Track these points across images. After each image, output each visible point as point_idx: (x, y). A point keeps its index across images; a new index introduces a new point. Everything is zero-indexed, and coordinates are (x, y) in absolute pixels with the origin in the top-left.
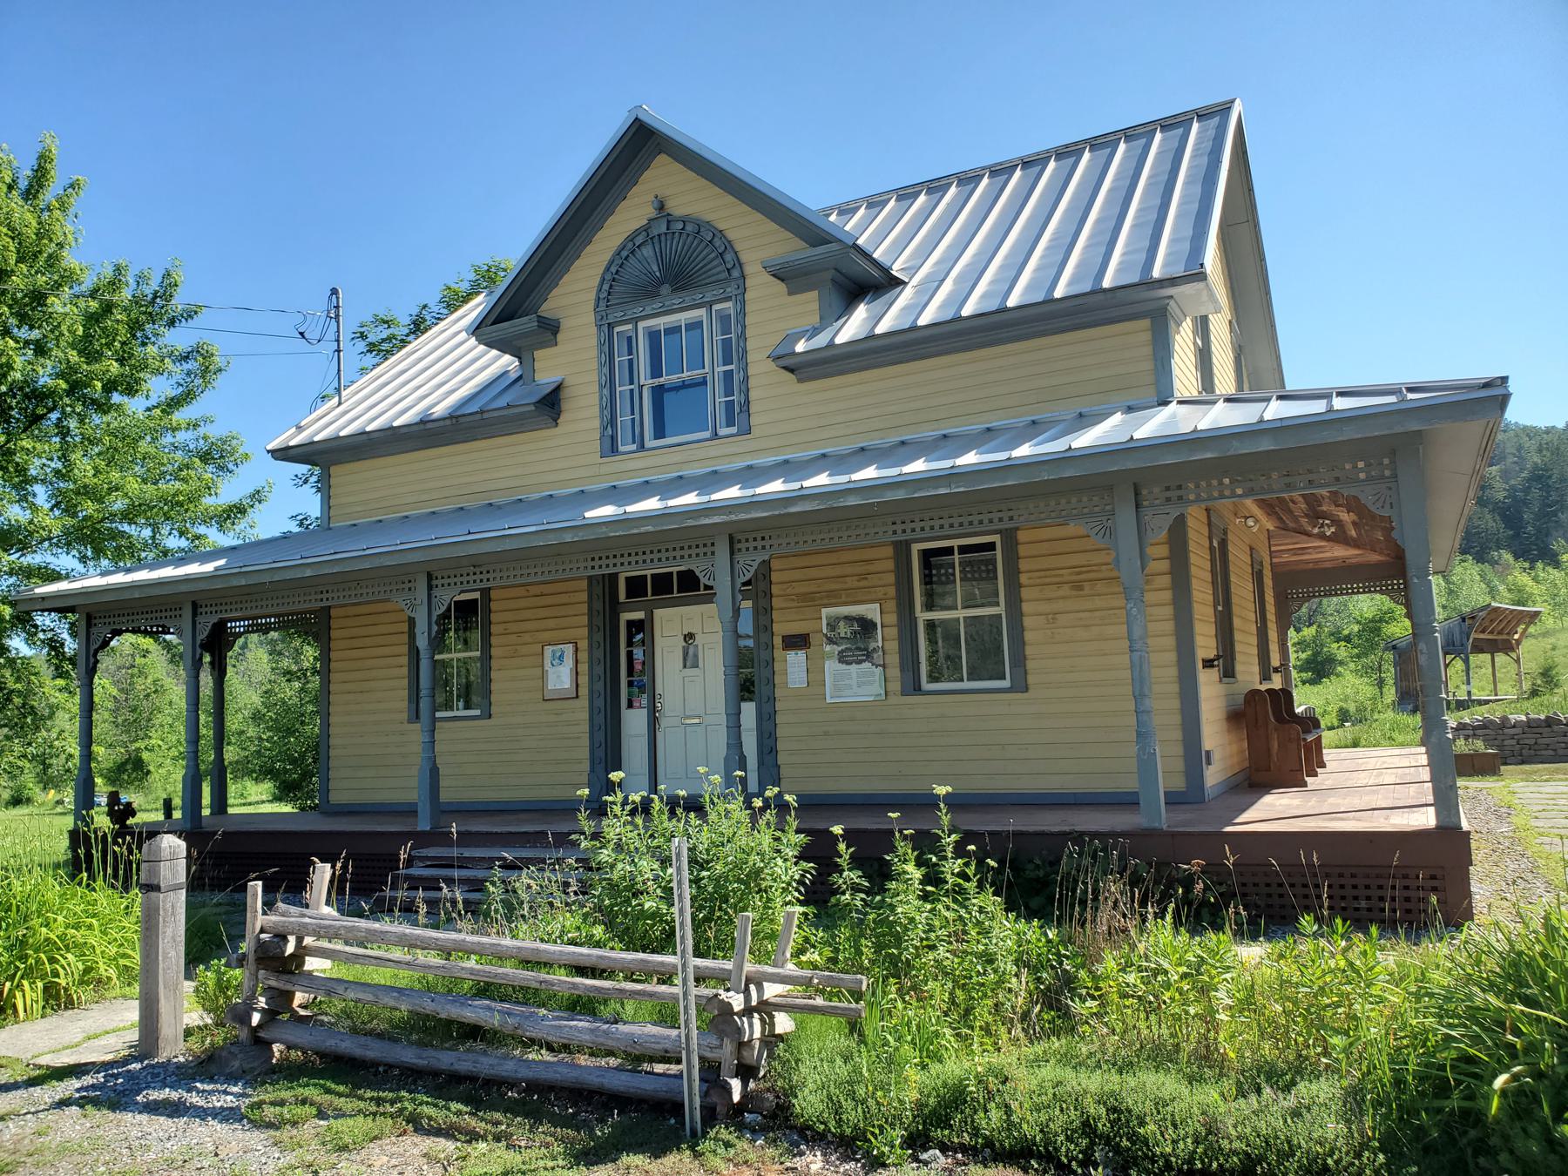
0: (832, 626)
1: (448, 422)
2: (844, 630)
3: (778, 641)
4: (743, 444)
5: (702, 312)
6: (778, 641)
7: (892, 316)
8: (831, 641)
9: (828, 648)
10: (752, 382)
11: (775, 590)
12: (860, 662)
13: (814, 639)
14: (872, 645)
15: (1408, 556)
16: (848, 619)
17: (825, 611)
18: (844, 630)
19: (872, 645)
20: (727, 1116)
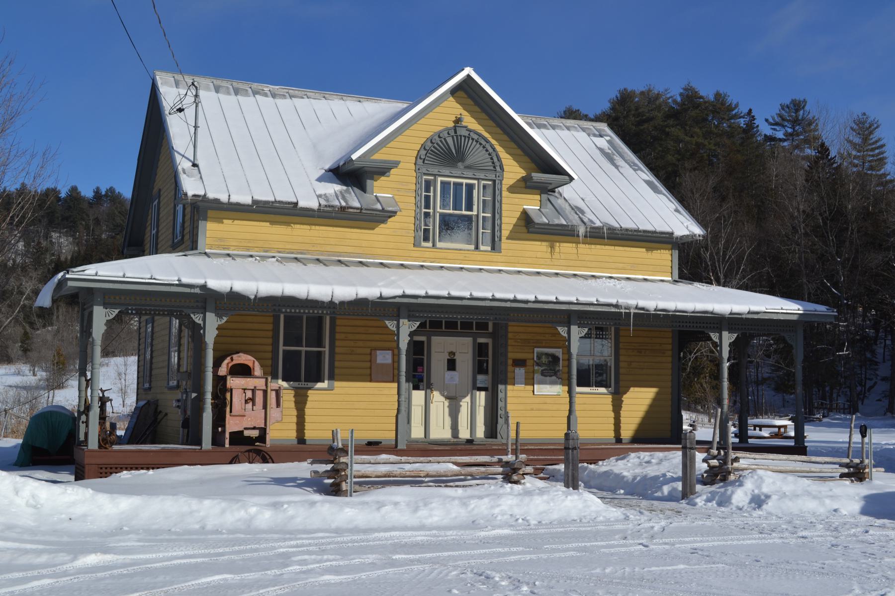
0: (539, 357)
1: (197, 291)
2: (544, 360)
3: (510, 362)
4: (495, 256)
5: (475, 182)
6: (510, 362)
7: (612, 364)
8: (538, 365)
9: (536, 368)
10: (503, 226)
11: (510, 335)
12: (551, 376)
13: (529, 363)
14: (557, 369)
15: (652, 192)
16: (547, 355)
17: (536, 350)
18: (544, 360)
19: (557, 369)
20: (547, 190)
